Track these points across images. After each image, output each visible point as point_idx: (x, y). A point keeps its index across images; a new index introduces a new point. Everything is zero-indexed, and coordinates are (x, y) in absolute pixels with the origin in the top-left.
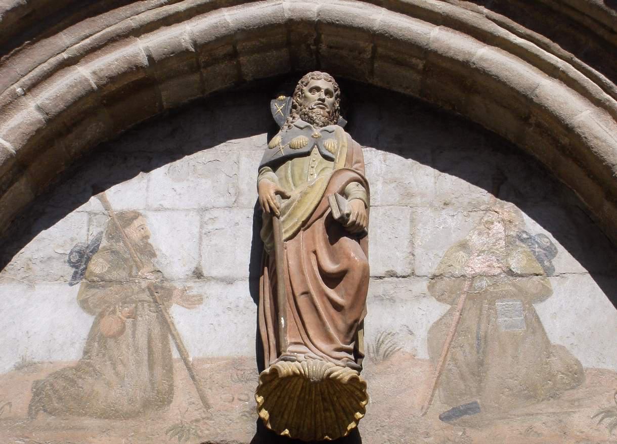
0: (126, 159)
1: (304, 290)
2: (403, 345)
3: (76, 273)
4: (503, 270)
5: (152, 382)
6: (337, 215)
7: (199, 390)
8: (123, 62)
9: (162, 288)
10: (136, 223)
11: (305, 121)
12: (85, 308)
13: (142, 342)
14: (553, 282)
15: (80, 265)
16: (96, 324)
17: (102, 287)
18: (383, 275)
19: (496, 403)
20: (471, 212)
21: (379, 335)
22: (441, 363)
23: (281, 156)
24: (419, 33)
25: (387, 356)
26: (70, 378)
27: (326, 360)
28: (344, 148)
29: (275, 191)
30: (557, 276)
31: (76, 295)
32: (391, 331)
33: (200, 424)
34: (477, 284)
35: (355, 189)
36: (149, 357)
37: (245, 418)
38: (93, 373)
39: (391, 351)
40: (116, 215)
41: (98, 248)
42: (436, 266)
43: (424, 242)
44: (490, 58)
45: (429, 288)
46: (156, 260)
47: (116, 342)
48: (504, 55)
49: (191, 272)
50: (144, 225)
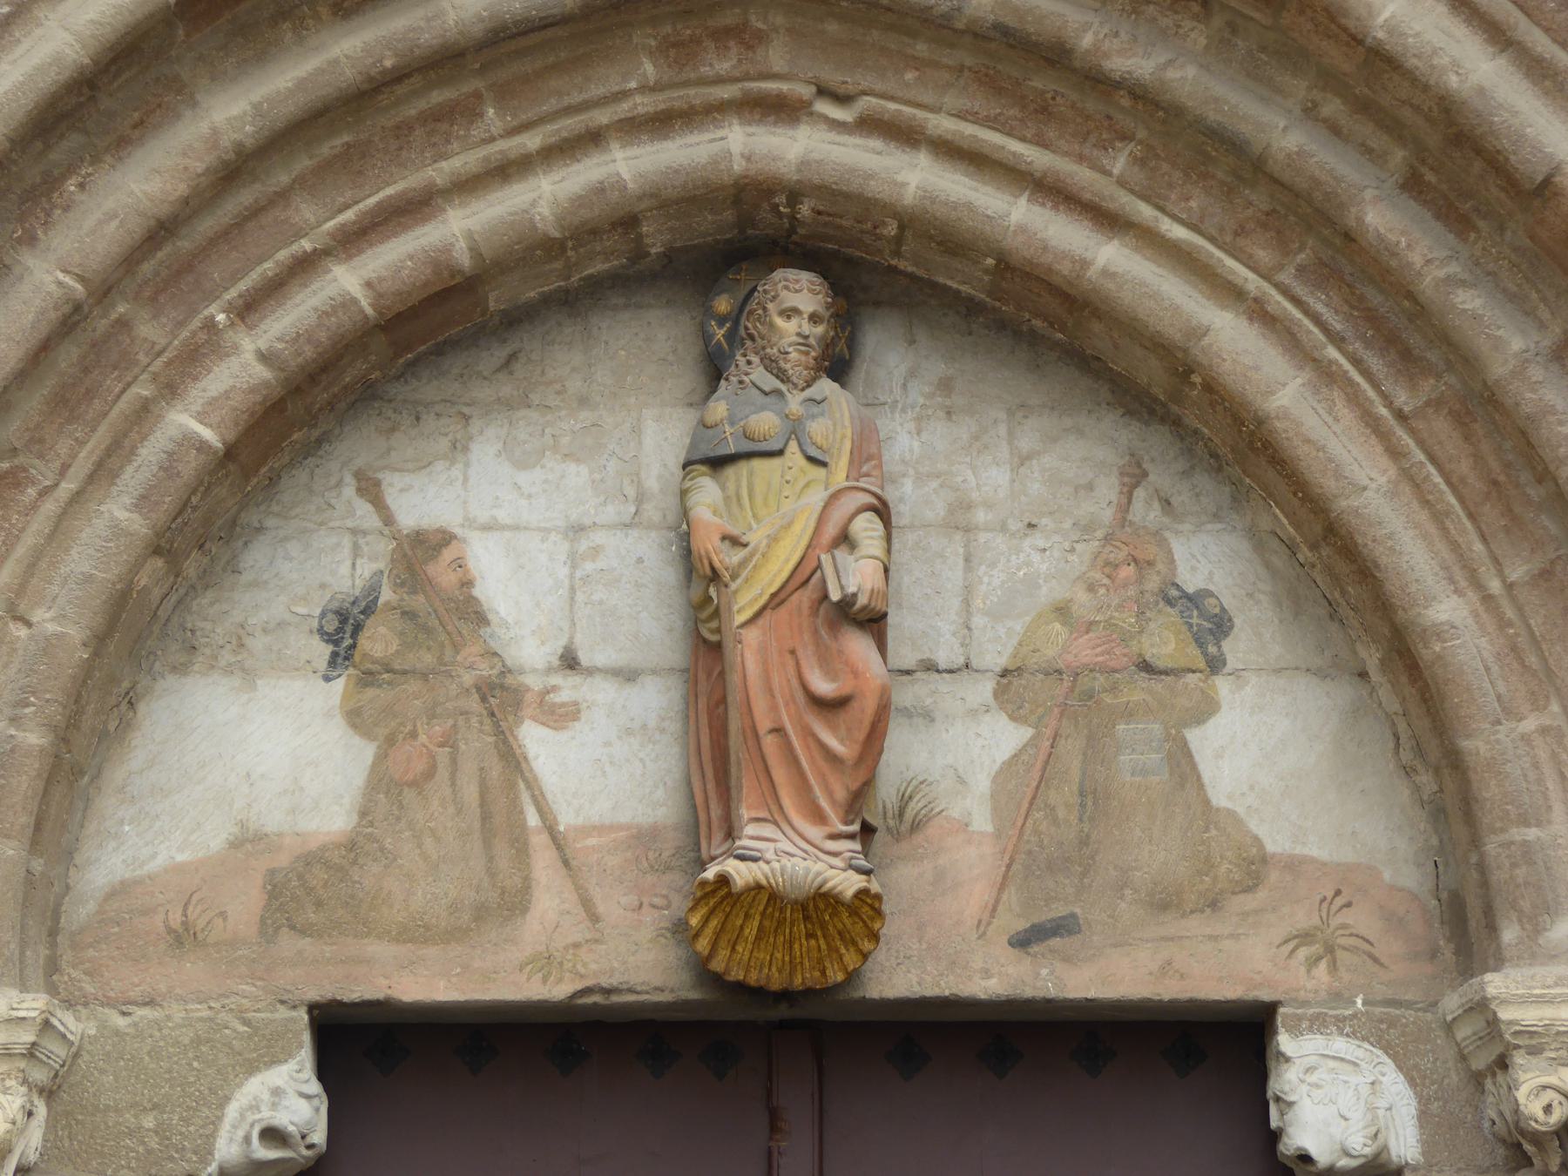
0: (418, 419)
1: (776, 726)
3: (335, 655)
5: (492, 873)
6: (835, 596)
9: (502, 687)
10: (448, 555)
12: (356, 727)
13: (470, 793)
14: (1222, 685)
15: (343, 638)
16: (381, 757)
17: (389, 683)
18: (914, 668)
19: (1109, 916)
20: (1077, 542)
21: (905, 784)
23: (728, 452)
24: (988, 216)
26: (335, 864)
27: (815, 859)
29: (720, 536)
30: (1230, 674)
31: (337, 700)
32: (925, 776)
35: (867, 528)
36: (483, 825)
38: (379, 854)
39: (925, 816)
41: (376, 605)
43: (988, 602)
44: (1120, 270)
48: (1147, 259)
49: (557, 657)
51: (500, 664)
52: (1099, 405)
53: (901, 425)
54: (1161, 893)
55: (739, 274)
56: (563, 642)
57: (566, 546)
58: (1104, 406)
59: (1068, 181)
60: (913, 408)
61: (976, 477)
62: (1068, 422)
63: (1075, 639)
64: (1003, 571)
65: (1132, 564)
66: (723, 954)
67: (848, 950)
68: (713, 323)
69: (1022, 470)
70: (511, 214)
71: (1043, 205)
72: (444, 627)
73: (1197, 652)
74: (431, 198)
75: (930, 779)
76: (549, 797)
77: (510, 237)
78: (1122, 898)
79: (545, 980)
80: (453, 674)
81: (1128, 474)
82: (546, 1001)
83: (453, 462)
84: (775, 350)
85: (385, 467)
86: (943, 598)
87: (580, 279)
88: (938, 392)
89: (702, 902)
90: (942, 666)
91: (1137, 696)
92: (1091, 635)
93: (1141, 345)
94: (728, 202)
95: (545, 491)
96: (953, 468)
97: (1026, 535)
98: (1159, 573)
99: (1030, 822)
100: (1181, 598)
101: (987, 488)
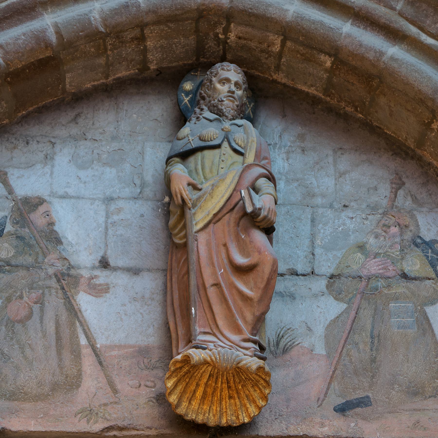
0: (28, 143)
1: (215, 282)
2: (302, 341)
4: (397, 272)
5: (61, 367)
6: (249, 209)
7: (106, 376)
8: (31, 38)
9: (69, 275)
10: (42, 209)
11: (214, 113)
13: (51, 328)
17: (8, 271)
18: (285, 273)
19: (386, 398)
21: (279, 330)
22: (336, 359)
24: (331, 28)
25: (287, 350)
27: (236, 349)
28: (253, 143)
29: (187, 182)
33: (109, 408)
34: (373, 284)
36: (57, 343)
37: (151, 403)
39: (290, 346)
40: (20, 199)
42: (334, 266)
43: (323, 242)
44: (400, 58)
45: (327, 287)
46: (62, 247)
47: (23, 326)
48: (413, 56)
50: (49, 211)
51: (68, 264)
52: (380, 149)
53: (279, 155)
54: (413, 387)
55: (197, 73)
56: (101, 254)
57: (104, 207)
58: (382, 150)
59: (373, 12)
60: (285, 147)
61: (317, 182)
62: (364, 157)
63: (368, 262)
64: (331, 227)
65: (397, 226)
66: (185, 404)
67: (251, 405)
68: (183, 94)
69: (341, 179)
70: (78, 15)
71: (359, 27)
72: (38, 245)
73: (431, 269)
74: (35, 7)
75: (293, 328)
76: (92, 330)
77: (77, 27)
78: (393, 389)
79: (88, 421)
80: (43, 267)
81: (395, 183)
82: (89, 433)
83: (46, 164)
84: (216, 101)
85: (9, 166)
86: (300, 239)
87: (114, 79)
88: (298, 140)
89: (174, 375)
90: (300, 272)
91: (400, 290)
92: (377, 260)
93: (406, 109)
94: (193, 31)
95: (93, 180)
96: (306, 177)
97: (343, 210)
98: (411, 231)
99: (345, 349)
100: (422, 244)
101: (323, 187)
